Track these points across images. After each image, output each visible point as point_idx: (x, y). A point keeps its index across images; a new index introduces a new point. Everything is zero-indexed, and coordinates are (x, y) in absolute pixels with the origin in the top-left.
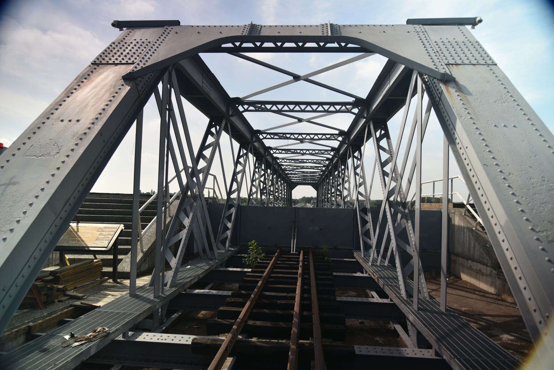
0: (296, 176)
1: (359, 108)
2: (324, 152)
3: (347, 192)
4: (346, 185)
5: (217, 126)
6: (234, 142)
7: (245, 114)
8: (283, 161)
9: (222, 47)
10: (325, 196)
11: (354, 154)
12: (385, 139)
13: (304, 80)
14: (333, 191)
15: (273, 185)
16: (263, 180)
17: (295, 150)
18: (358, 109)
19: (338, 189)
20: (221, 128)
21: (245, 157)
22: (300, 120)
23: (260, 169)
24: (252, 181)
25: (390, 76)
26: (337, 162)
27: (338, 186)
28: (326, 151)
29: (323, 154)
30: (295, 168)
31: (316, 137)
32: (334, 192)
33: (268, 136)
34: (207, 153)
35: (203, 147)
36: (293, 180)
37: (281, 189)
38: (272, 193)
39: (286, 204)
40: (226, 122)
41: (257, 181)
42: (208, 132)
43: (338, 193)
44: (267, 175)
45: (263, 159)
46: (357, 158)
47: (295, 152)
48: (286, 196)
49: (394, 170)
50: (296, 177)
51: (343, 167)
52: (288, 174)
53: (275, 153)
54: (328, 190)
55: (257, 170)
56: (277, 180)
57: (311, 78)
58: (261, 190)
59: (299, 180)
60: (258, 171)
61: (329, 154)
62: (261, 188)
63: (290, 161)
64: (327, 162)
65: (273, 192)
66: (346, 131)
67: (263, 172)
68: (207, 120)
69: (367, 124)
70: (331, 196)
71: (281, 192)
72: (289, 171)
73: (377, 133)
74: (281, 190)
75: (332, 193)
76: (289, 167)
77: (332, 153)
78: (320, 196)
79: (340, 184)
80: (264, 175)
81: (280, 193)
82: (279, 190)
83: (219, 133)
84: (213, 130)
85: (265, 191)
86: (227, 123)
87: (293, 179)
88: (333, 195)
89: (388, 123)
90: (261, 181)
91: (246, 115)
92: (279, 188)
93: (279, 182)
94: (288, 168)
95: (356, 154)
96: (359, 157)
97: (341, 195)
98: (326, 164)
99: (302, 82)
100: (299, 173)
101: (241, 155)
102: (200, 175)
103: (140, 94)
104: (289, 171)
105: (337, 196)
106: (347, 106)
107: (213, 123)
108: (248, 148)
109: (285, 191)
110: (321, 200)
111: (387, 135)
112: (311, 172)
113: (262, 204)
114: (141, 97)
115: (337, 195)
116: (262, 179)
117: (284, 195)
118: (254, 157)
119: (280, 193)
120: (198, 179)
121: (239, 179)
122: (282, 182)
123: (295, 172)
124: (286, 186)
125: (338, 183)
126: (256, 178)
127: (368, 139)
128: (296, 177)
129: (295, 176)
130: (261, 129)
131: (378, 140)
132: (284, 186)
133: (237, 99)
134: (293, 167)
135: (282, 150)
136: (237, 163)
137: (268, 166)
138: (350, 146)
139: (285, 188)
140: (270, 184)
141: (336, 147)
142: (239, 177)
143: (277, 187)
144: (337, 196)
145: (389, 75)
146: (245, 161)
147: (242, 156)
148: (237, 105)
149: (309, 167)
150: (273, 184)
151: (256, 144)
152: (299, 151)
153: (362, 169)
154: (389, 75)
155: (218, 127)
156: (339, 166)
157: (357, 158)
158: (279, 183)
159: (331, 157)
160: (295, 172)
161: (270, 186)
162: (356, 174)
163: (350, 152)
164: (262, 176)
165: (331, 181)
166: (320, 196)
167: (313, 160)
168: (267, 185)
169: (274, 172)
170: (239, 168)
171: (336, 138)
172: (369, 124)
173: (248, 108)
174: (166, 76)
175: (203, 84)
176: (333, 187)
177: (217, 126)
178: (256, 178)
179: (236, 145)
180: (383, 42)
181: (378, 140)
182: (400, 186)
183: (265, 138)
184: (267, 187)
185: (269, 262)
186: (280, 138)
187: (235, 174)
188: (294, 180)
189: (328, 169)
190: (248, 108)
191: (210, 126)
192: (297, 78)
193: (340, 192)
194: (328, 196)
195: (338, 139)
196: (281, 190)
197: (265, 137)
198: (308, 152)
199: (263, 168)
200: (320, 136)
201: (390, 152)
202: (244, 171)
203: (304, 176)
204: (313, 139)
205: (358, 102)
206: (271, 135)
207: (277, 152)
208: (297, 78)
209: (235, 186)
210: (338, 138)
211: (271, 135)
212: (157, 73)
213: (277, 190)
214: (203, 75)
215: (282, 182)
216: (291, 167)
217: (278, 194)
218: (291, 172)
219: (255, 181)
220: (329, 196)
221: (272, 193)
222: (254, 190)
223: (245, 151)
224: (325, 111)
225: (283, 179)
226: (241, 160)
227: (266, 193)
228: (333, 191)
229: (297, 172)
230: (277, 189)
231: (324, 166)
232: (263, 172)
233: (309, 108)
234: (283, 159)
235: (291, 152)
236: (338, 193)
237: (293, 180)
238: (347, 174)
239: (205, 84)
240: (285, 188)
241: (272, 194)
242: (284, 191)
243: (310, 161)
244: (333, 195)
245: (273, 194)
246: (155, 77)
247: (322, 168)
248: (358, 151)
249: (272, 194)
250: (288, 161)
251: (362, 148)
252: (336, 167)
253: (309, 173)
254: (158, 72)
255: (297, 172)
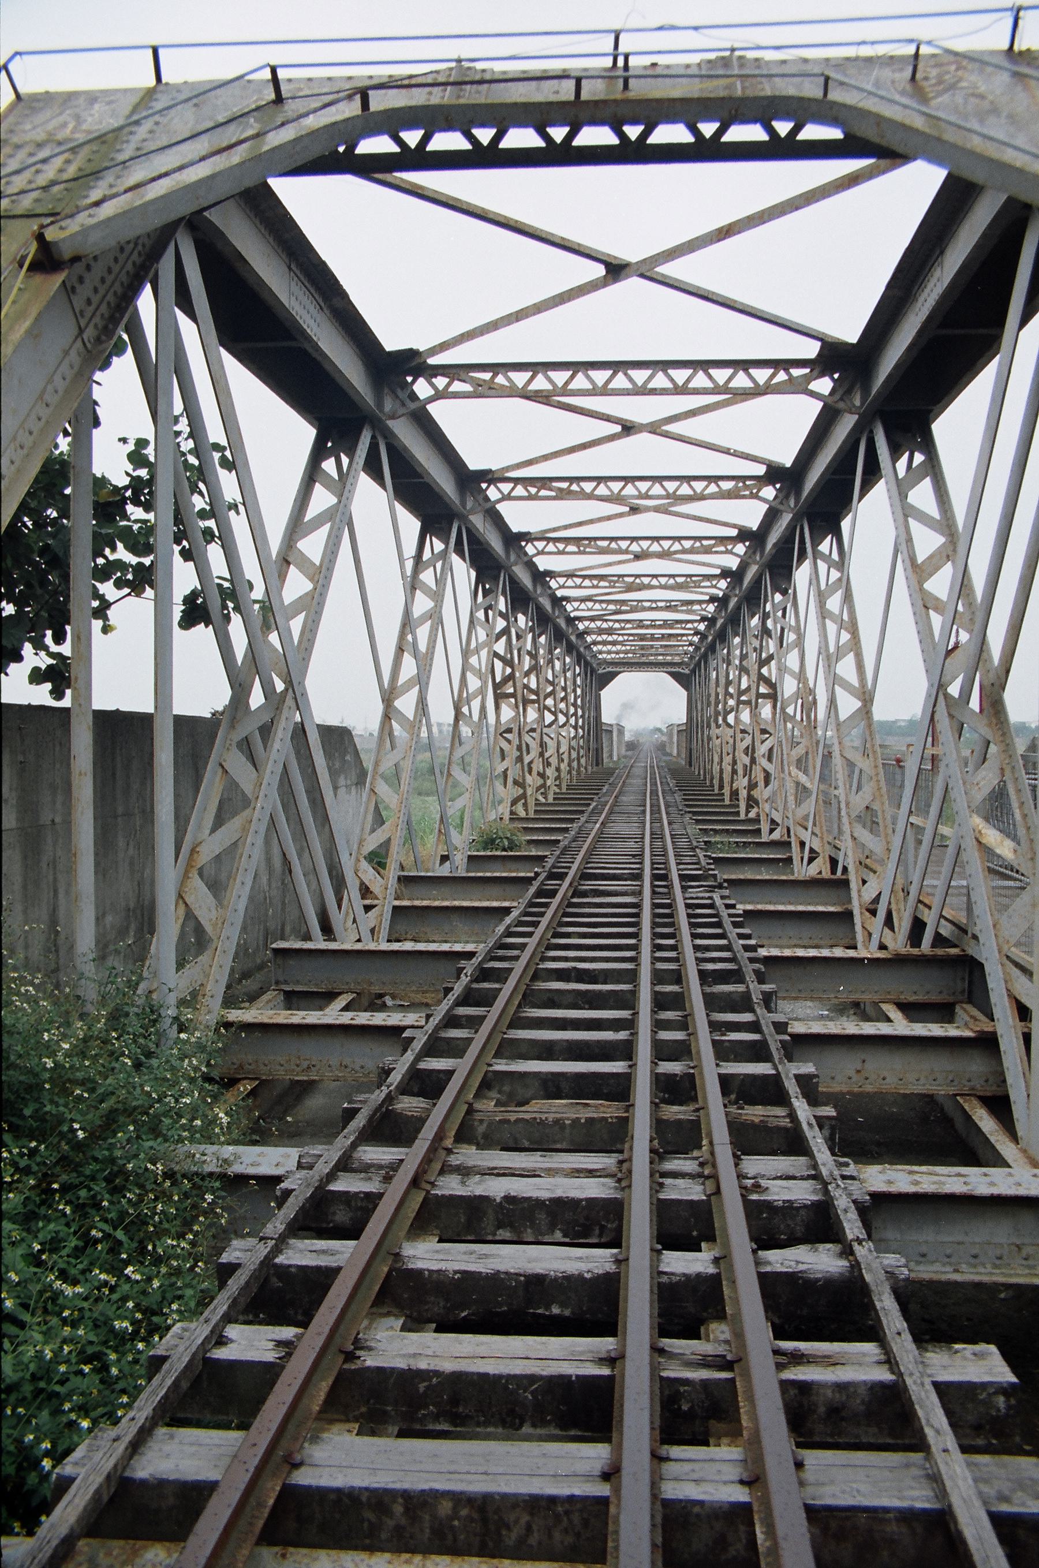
0: (615, 637)
1: (836, 376)
2: (714, 546)
3: (796, 682)
4: (792, 660)
5: (343, 456)
6: (403, 513)
7: (435, 409)
8: (570, 583)
9: (358, 155)
10: (717, 705)
11: (819, 548)
12: (927, 482)
13: (642, 276)
14: (744, 685)
15: (536, 669)
16: (502, 653)
17: (612, 539)
18: (833, 379)
19: (761, 678)
20: (354, 465)
21: (439, 565)
22: (628, 429)
23: (490, 613)
24: (466, 653)
25: (942, 253)
26: (758, 581)
27: (761, 667)
28: (722, 540)
29: (707, 551)
30: (612, 607)
31: (685, 490)
32: (748, 689)
33: (520, 491)
34: (312, 546)
35: (297, 526)
36: (605, 656)
37: (563, 684)
38: (534, 697)
39: (583, 737)
40: (373, 437)
41: (484, 653)
42: (312, 474)
43: (763, 690)
44: (517, 634)
45: (502, 575)
46: (827, 559)
47: (609, 545)
48: (582, 708)
49: (963, 585)
50: (614, 643)
51: (778, 597)
52: (587, 632)
53: (577, 609)
54: (728, 683)
55: (480, 614)
56: (551, 652)
57: (665, 269)
58: (496, 686)
59: (626, 652)
60: (483, 619)
61: (715, 587)
62: (498, 679)
63: (595, 582)
64: (711, 608)
65: (536, 693)
66: (734, 569)
67: (501, 624)
68: (306, 433)
69: (861, 433)
70: (739, 702)
71: (563, 694)
72: (592, 619)
73: (897, 465)
74: (564, 689)
75: (741, 693)
76: (590, 604)
77: (740, 549)
78: (699, 708)
79: (771, 658)
80: (505, 631)
81: (562, 700)
82: (558, 688)
83: (342, 486)
84: (329, 465)
85: (511, 690)
86: (378, 444)
87: (604, 652)
88: (743, 698)
89: (935, 427)
90: (496, 655)
91: (439, 411)
92: (556, 681)
93: (558, 659)
94: (589, 610)
95: (824, 547)
96: (835, 556)
97: (773, 697)
98: (720, 589)
99: (632, 284)
100: (623, 629)
101: (425, 558)
102: (291, 623)
103: (83, 325)
104: (592, 619)
105: (760, 700)
106: (791, 370)
107: (330, 444)
108: (450, 530)
109: (579, 691)
110: (703, 721)
111: (933, 467)
112: (666, 624)
113: (501, 734)
114: (85, 336)
115: (759, 696)
116: (500, 647)
117: (575, 705)
118: (471, 570)
119: (562, 700)
120: (285, 637)
121: (423, 647)
122: (568, 660)
123: (611, 624)
124: (579, 674)
125: (761, 655)
126: (480, 641)
127: (867, 486)
128: (614, 643)
129: (610, 639)
130: (494, 465)
131: (902, 489)
132: (575, 676)
133: (411, 354)
134: (604, 606)
135: (567, 540)
136: (413, 585)
137: (520, 600)
138: (802, 521)
139: (579, 682)
140: (526, 667)
141: (754, 524)
142: (423, 633)
143: (550, 678)
144: (760, 700)
145: (938, 252)
146: (440, 582)
147: (432, 563)
148: (409, 375)
149: (660, 604)
150: (535, 668)
151: (478, 521)
152: (624, 544)
153: (848, 598)
154: (938, 252)
155: (345, 460)
156: (766, 595)
157: (827, 559)
158: (557, 664)
159: (733, 563)
160: (611, 624)
161: (527, 674)
162: (824, 614)
163: (802, 541)
164: (498, 637)
165: (738, 652)
166: (699, 708)
167: (673, 576)
168: (516, 668)
169: (542, 621)
170: (422, 604)
171: (755, 491)
172: (871, 432)
173: (449, 385)
174: (166, 267)
175: (293, 299)
176: (743, 669)
177: (343, 456)
178: (480, 641)
179: (411, 525)
180: (215, 1466)
181: (902, 489)
182: (981, 650)
183: (440, 395)
184: (517, 674)
185: (543, 910)
186: (563, 495)
187: (407, 624)
188: (609, 652)
189: (726, 610)
190: (449, 385)
191: (318, 453)
192: (616, 270)
193: (772, 686)
194: (726, 703)
195: (734, 551)
196: (564, 689)
197: (506, 493)
198: (655, 547)
199: (502, 606)
200: (699, 486)
201: (946, 524)
202: (435, 617)
203: (642, 638)
204: (565, 391)
205: (774, 474)
206: (529, 488)
207: (551, 547)
208: (616, 270)
209: (409, 667)
210: (759, 491)
211: (529, 488)
212: (136, 252)
213: (550, 689)
214: (290, 269)
215: (568, 660)
216: (597, 606)
217: (555, 700)
218: (599, 623)
219: (477, 651)
220: (731, 702)
221: (534, 697)
222: (474, 683)
223: (439, 546)
224: (723, 389)
225: (570, 649)
226: (427, 577)
227: (513, 695)
228: (744, 685)
229: (617, 625)
230: (552, 683)
231: (703, 619)
232: (501, 624)
233: (660, 381)
234: (570, 575)
235: (598, 547)
236: (763, 690)
237: (605, 656)
238: (793, 623)
239: (299, 298)
240: (579, 682)
241: (533, 702)
242: (574, 691)
243: (663, 580)
244: (743, 698)
245: (537, 701)
246: (129, 266)
247: (704, 606)
248: (830, 536)
249: (533, 702)
250: (587, 583)
251: (845, 524)
252: (753, 599)
253: (660, 627)
254: (140, 248)
255: (617, 625)
